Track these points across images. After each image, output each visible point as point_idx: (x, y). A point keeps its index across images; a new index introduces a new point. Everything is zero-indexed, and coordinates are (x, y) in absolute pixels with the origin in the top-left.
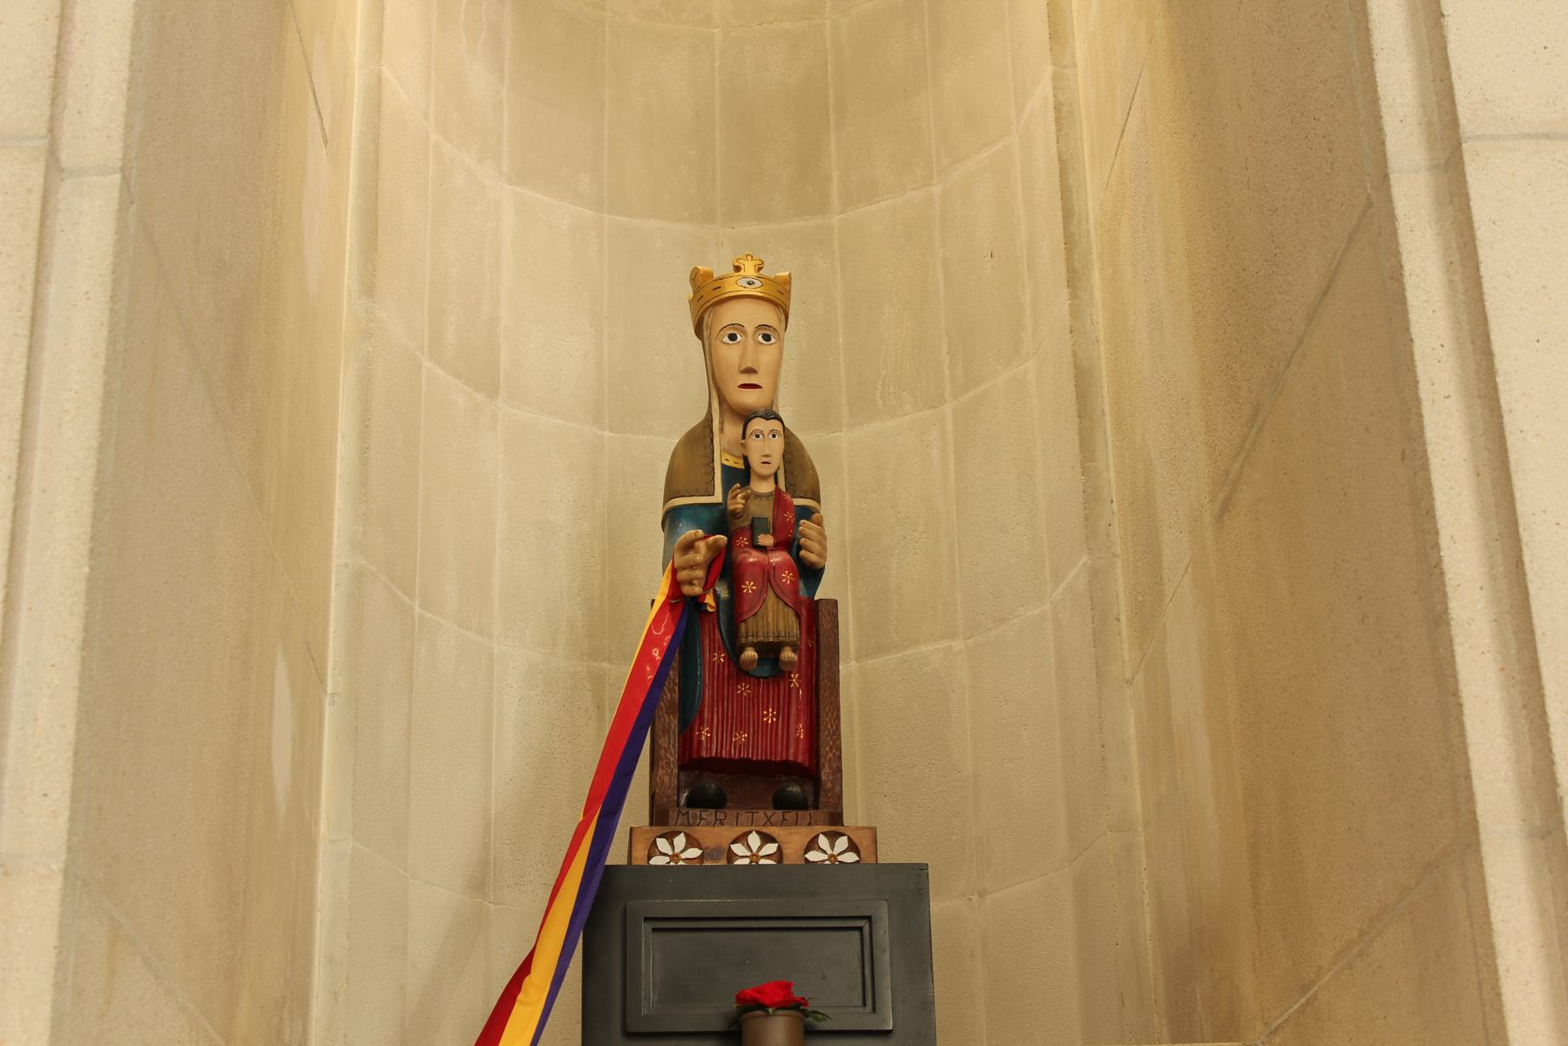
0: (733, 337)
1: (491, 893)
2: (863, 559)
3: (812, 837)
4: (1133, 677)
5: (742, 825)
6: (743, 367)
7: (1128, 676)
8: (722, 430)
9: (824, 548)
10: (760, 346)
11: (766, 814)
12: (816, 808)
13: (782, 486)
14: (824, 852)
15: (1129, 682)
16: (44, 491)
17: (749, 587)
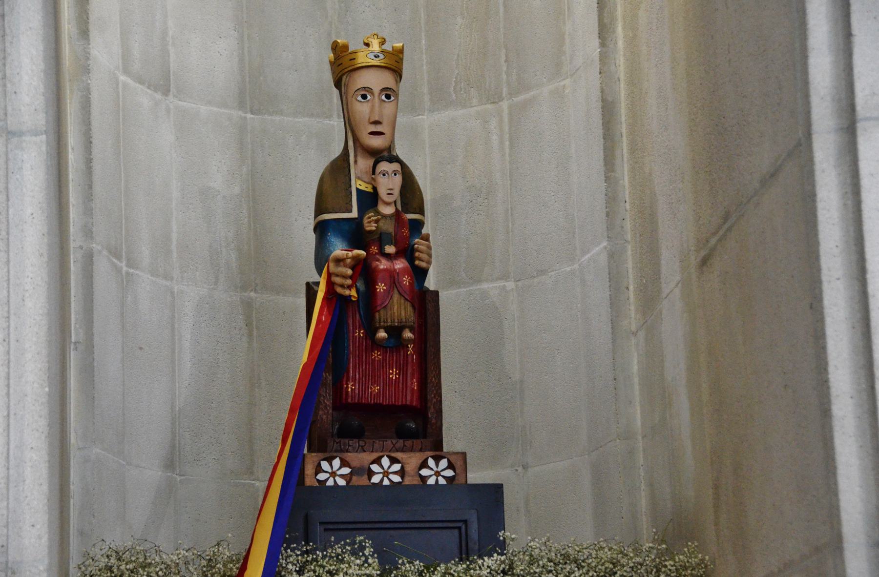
0: (364, 97)
1: (177, 468)
2: (440, 215)
3: (423, 459)
4: (637, 332)
5: (376, 451)
6: (372, 120)
7: (634, 328)
8: (356, 162)
9: (430, 256)
10: (384, 103)
11: (392, 443)
12: (425, 437)
13: (400, 208)
14: (432, 469)
15: (635, 334)
16: (17, 341)
17: (381, 287)
